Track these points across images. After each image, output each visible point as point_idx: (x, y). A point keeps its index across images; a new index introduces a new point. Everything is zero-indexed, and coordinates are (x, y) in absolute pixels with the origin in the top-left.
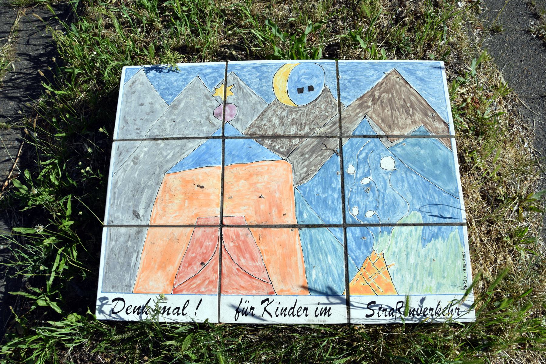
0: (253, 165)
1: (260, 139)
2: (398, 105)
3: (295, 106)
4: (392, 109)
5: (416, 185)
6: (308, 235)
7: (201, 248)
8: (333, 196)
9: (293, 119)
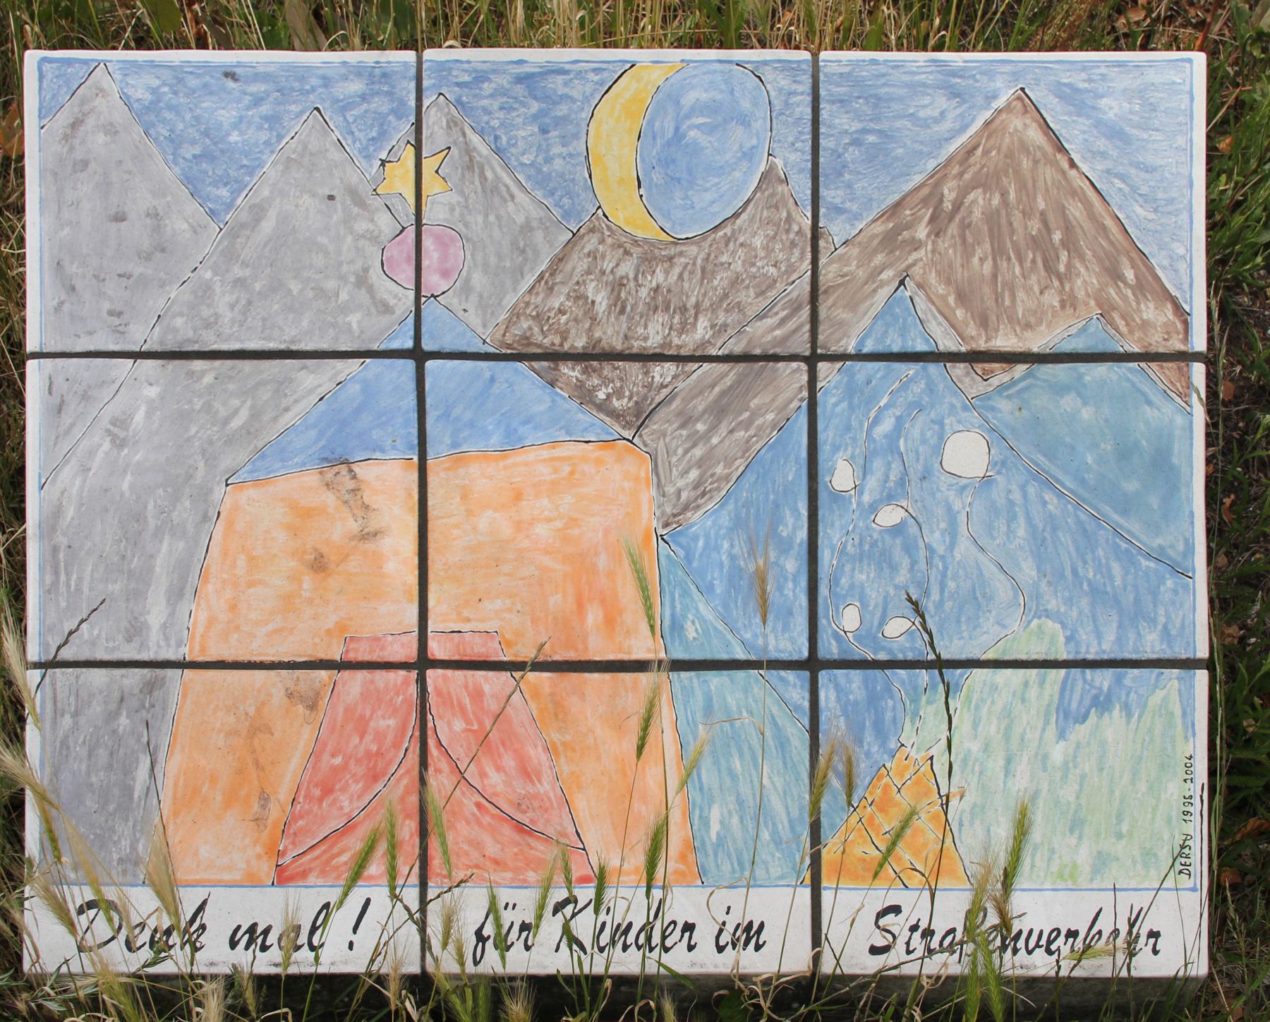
0: (519, 458)
1: (545, 364)
2: (1019, 237)
3: (664, 237)
4: (998, 252)
5: (1055, 529)
6: (698, 692)
7: (362, 737)
8: (782, 568)
9: (657, 289)
